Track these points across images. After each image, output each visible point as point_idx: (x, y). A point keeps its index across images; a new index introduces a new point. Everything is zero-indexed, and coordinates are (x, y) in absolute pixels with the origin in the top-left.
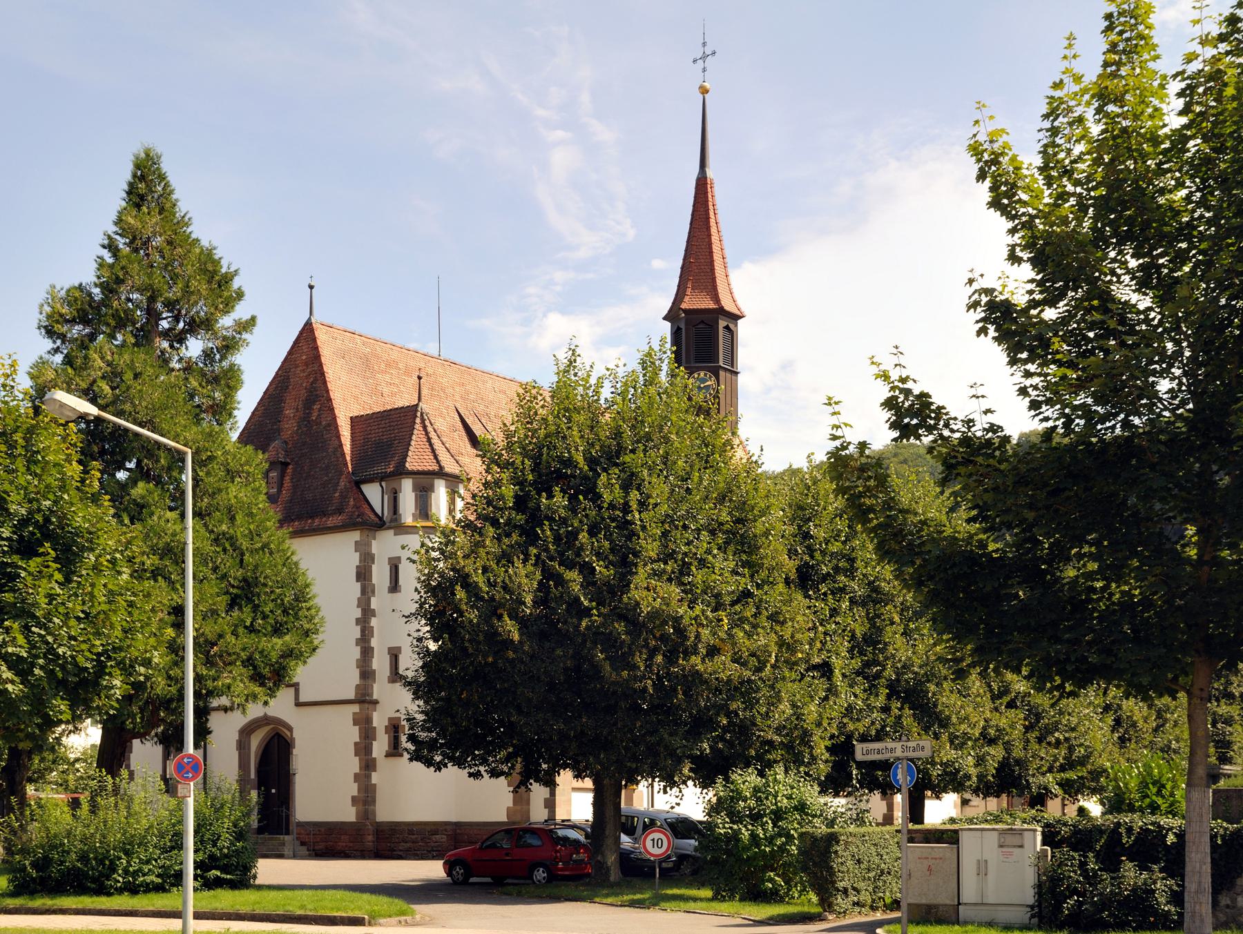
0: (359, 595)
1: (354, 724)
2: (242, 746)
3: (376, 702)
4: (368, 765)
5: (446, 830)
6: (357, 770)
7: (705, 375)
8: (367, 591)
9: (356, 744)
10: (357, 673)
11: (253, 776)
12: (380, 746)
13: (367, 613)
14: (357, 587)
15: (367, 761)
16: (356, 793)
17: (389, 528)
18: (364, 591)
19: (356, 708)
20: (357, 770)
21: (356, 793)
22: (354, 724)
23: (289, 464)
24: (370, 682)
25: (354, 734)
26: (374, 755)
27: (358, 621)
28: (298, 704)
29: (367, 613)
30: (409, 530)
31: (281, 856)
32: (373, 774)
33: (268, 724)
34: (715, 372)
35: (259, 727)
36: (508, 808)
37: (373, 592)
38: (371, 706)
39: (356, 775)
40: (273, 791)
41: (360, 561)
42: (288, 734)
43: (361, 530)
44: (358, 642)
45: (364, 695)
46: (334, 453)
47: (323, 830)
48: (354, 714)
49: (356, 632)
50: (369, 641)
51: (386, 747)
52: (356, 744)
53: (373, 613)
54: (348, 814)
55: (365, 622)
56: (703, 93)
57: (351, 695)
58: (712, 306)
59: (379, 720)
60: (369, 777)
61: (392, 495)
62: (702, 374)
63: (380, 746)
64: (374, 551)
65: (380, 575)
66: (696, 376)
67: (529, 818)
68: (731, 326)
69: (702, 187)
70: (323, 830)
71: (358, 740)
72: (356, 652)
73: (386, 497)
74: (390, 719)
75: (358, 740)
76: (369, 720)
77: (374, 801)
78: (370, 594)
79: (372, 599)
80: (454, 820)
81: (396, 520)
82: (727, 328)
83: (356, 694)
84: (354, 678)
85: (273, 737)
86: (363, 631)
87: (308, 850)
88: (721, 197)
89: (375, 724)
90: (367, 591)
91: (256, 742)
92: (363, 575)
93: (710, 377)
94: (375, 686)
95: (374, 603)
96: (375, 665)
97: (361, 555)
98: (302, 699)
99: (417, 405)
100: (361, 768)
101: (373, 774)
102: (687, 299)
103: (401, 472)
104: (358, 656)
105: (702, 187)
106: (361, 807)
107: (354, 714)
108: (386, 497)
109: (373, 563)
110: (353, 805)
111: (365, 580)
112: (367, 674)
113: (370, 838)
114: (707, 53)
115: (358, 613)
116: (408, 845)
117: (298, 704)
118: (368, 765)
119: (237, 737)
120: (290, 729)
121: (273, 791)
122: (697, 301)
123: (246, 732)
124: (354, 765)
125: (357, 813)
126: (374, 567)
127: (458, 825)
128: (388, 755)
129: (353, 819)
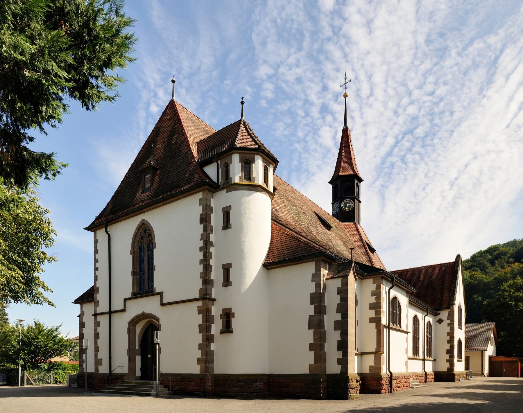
0: (202, 232)
1: (199, 314)
2: (131, 331)
3: (214, 300)
4: (208, 339)
5: (263, 379)
6: (201, 342)
7: (349, 201)
8: (207, 230)
9: (200, 326)
10: (200, 281)
11: (137, 347)
12: (216, 328)
13: (207, 244)
14: (200, 228)
15: (208, 336)
16: (200, 356)
17: (222, 189)
18: (205, 229)
19: (200, 303)
20: (201, 342)
21: (200, 356)
22: (199, 314)
23: (158, 169)
24: (210, 287)
25: (199, 319)
26: (213, 332)
27: (201, 249)
28: (162, 304)
29: (207, 244)
30: (237, 187)
31: (149, 395)
32: (212, 344)
33: (145, 318)
34: (353, 199)
35: (140, 320)
36: (310, 365)
37: (212, 231)
38: (210, 302)
39: (200, 345)
40: (149, 356)
41: (203, 211)
42: (157, 322)
43: (203, 190)
44: (201, 262)
45: (205, 294)
46: (185, 155)
47: (178, 378)
48: (198, 307)
49: (200, 256)
50: (209, 261)
51: (220, 327)
52: (200, 326)
53: (212, 244)
54: (195, 369)
55: (206, 248)
56: (345, 97)
57: (197, 296)
58: (352, 173)
59: (216, 311)
60: (209, 346)
61: (225, 169)
62: (348, 200)
63: (216, 328)
64: (212, 205)
65: (216, 219)
66: (345, 201)
67: (325, 371)
68: (359, 183)
69: (346, 133)
70: (178, 378)
71: (201, 323)
72: (200, 269)
73: (220, 170)
74: (223, 310)
75: (201, 323)
76: (209, 311)
77: (212, 361)
78: (209, 231)
79: (211, 235)
80: (267, 372)
81: (228, 183)
82: (357, 183)
83: (200, 294)
84: (199, 284)
85: (149, 326)
86: (205, 255)
87: (169, 390)
88: (353, 136)
89: (213, 313)
90: (207, 230)
91: (139, 329)
92: (205, 219)
93: (351, 201)
94: (213, 290)
95: (212, 238)
96: (213, 276)
97: (203, 207)
98: (165, 301)
99: (240, 120)
100: (203, 340)
101: (212, 344)
102: (341, 172)
103: (233, 149)
104: (201, 270)
105: (346, 133)
106: (203, 365)
107: (198, 307)
108: (220, 170)
109: (212, 213)
110: (198, 364)
111: (206, 221)
112: (207, 281)
113: (210, 384)
114: (347, 81)
115: (201, 244)
116: (237, 389)
117: (162, 304)
118: (208, 339)
119: (127, 326)
120: (158, 319)
121: (149, 356)
122: (345, 171)
123: (133, 323)
124: (199, 339)
125: (201, 368)
126: (212, 216)
127: (270, 376)
128: (222, 332)
129: (369, 372)
